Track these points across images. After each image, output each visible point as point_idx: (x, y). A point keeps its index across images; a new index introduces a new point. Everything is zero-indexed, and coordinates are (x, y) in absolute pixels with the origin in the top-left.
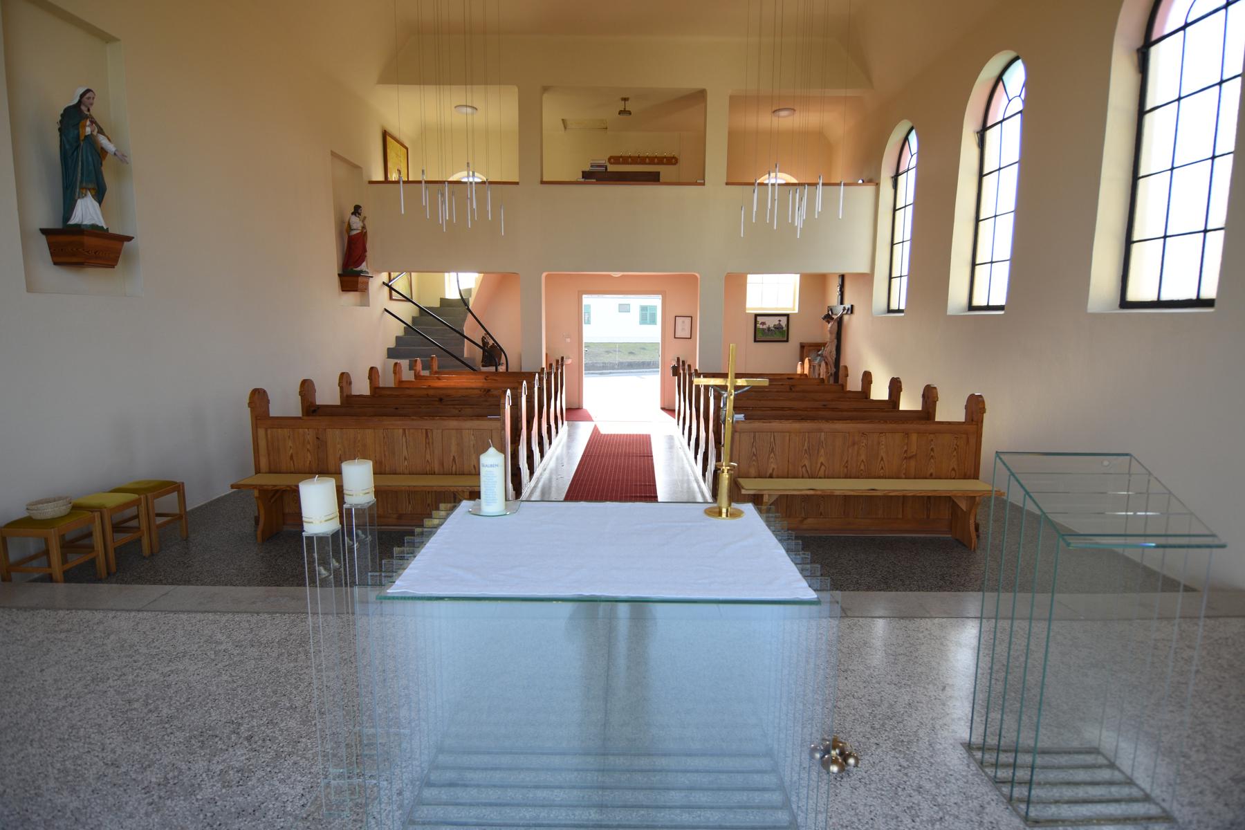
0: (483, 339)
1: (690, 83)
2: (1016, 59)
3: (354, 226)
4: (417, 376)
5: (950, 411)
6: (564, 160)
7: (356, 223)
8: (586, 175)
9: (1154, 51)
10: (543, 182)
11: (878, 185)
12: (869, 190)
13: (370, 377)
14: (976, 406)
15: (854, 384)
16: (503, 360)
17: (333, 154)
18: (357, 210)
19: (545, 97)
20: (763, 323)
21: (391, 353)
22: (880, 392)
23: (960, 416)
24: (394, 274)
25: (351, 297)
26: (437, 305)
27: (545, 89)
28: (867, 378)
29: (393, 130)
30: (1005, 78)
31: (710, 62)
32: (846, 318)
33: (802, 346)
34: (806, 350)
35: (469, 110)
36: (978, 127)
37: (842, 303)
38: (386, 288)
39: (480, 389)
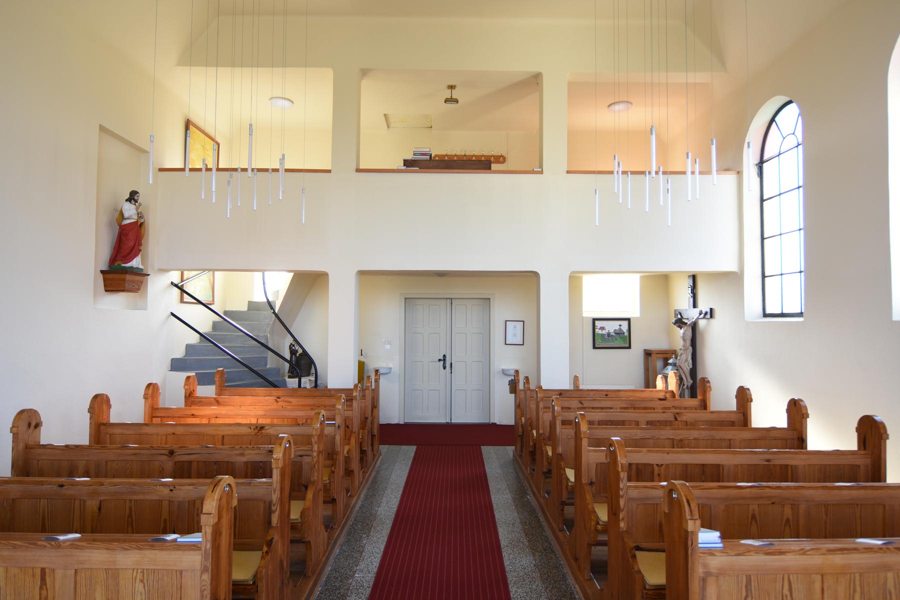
0: (291, 346)
1: (526, 66)
2: (790, 102)
3: (126, 215)
4: (190, 398)
5: (769, 414)
6: (384, 149)
7: (130, 211)
8: (408, 163)
9: (765, 165)
10: (358, 170)
11: (739, 173)
12: (730, 179)
13: (91, 410)
14: (871, 432)
15: (723, 400)
16: (313, 371)
17: (102, 129)
18: (133, 197)
19: (365, 84)
20: (602, 328)
21: (177, 365)
22: (769, 414)
23: (782, 422)
24: (187, 274)
25: (119, 299)
26: (245, 308)
27: (364, 72)
28: (744, 396)
29: (194, 119)
30: (776, 119)
31: (549, 46)
32: (702, 323)
33: (648, 354)
34: (655, 361)
35: (287, 103)
36: (757, 161)
37: (695, 306)
38: (177, 291)
39: (249, 426)
